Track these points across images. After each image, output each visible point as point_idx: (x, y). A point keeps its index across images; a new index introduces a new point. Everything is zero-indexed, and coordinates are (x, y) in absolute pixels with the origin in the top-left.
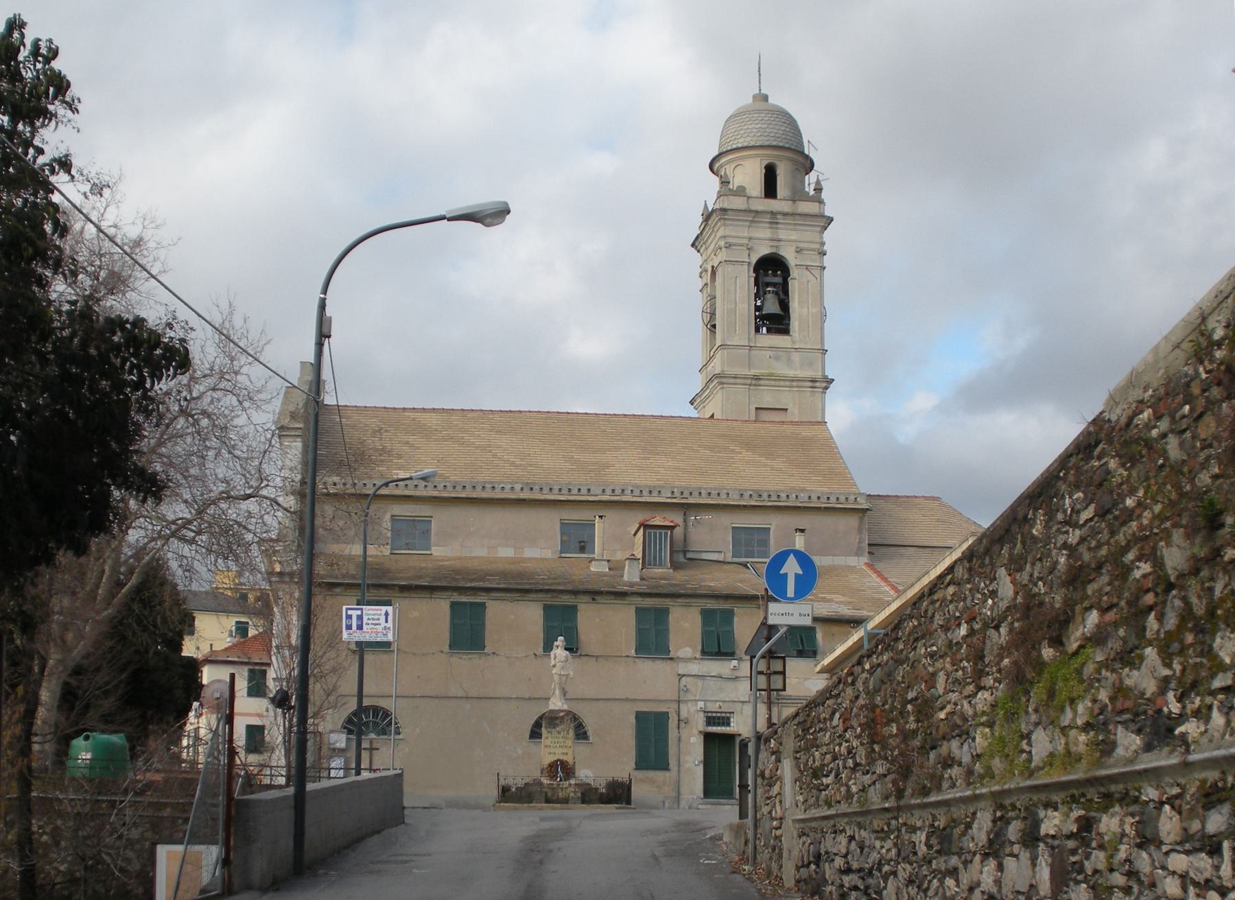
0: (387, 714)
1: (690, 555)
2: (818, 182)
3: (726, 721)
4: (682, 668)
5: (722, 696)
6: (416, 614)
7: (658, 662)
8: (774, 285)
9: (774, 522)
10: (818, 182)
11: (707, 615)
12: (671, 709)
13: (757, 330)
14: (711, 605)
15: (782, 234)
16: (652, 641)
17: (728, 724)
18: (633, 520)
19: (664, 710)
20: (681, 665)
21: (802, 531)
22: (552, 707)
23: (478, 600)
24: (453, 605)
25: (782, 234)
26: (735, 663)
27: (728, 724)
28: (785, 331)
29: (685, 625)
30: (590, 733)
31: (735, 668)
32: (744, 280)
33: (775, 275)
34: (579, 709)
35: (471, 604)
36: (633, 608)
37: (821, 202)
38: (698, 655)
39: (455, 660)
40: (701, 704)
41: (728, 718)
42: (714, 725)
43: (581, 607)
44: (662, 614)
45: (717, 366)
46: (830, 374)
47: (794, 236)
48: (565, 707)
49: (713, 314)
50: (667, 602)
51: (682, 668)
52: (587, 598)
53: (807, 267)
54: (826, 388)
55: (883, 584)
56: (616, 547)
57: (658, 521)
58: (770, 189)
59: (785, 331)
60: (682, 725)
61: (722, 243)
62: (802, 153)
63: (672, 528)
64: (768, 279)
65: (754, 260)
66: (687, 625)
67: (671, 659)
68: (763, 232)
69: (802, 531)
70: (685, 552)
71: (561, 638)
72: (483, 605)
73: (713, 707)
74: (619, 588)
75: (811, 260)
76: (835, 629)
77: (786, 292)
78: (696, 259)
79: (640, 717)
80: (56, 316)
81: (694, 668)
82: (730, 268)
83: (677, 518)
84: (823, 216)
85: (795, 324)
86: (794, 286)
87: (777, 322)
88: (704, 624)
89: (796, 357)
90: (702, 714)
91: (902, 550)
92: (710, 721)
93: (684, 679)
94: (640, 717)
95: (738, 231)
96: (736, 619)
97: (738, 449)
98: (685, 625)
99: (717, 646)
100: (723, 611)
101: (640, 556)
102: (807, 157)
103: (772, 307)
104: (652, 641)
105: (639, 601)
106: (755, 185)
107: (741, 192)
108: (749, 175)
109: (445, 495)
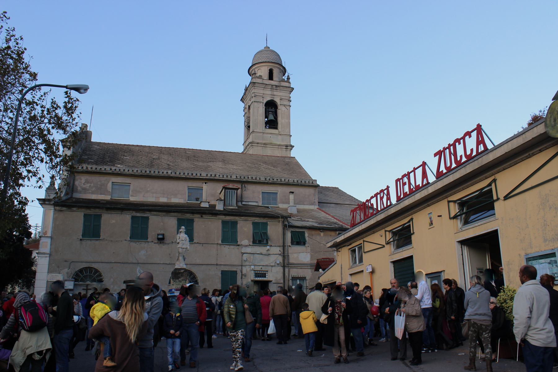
0: (97, 271)
1: (244, 203)
2: (288, 76)
3: (264, 275)
4: (244, 250)
5: (262, 263)
6: (114, 221)
7: (232, 247)
8: (272, 112)
9: (280, 190)
10: (288, 76)
11: (255, 224)
12: (238, 269)
13: (266, 127)
14: (257, 220)
15: (275, 93)
16: (229, 237)
17: (265, 277)
18: (219, 187)
19: (235, 269)
20: (244, 248)
21: (293, 193)
22: (177, 267)
23: (145, 215)
24: (133, 218)
25: (275, 93)
26: (268, 247)
27: (265, 277)
28: (276, 128)
29: (245, 228)
30: (199, 281)
31: (268, 250)
32: (261, 109)
33: (272, 108)
34: (194, 270)
35: (142, 217)
36: (221, 221)
37: (290, 83)
38: (251, 244)
39: (133, 244)
40: (252, 267)
41: (265, 274)
42: (259, 277)
43: (196, 220)
44: (235, 224)
45: (250, 140)
46: (292, 144)
47: (281, 94)
48: (185, 267)
49: (249, 123)
50: (237, 218)
51: (244, 250)
52: (199, 216)
53: (284, 105)
54: (291, 149)
55: (327, 215)
56: (210, 195)
57: (231, 186)
58: (271, 77)
59: (276, 128)
60: (243, 277)
61: (253, 95)
62: (282, 66)
63: (237, 189)
64: (270, 110)
65: (265, 102)
66: (246, 229)
67: (238, 245)
68: (268, 92)
69: (293, 193)
70: (242, 201)
71: (183, 227)
72: (147, 218)
73: (258, 268)
74: (214, 212)
75: (286, 103)
76: (313, 232)
77: (276, 115)
78: (243, 105)
79: (223, 272)
80: (43, 155)
81: (249, 250)
82: (256, 104)
83: (239, 186)
84: (290, 87)
85: (280, 126)
86: (279, 112)
87: (272, 124)
88: (254, 229)
89: (280, 137)
90: (253, 272)
91: (329, 205)
92: (257, 275)
93: (245, 255)
94: (223, 272)
95: (259, 91)
96: (269, 227)
97: (262, 164)
98: (245, 228)
99: (260, 238)
100: (263, 223)
101: (223, 198)
102: (284, 68)
103: (271, 117)
104: (229, 237)
105: (223, 217)
106: (266, 75)
107: (260, 77)
108: (263, 72)
109: (137, 174)
